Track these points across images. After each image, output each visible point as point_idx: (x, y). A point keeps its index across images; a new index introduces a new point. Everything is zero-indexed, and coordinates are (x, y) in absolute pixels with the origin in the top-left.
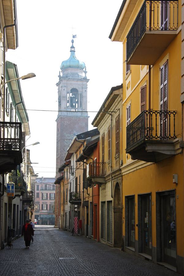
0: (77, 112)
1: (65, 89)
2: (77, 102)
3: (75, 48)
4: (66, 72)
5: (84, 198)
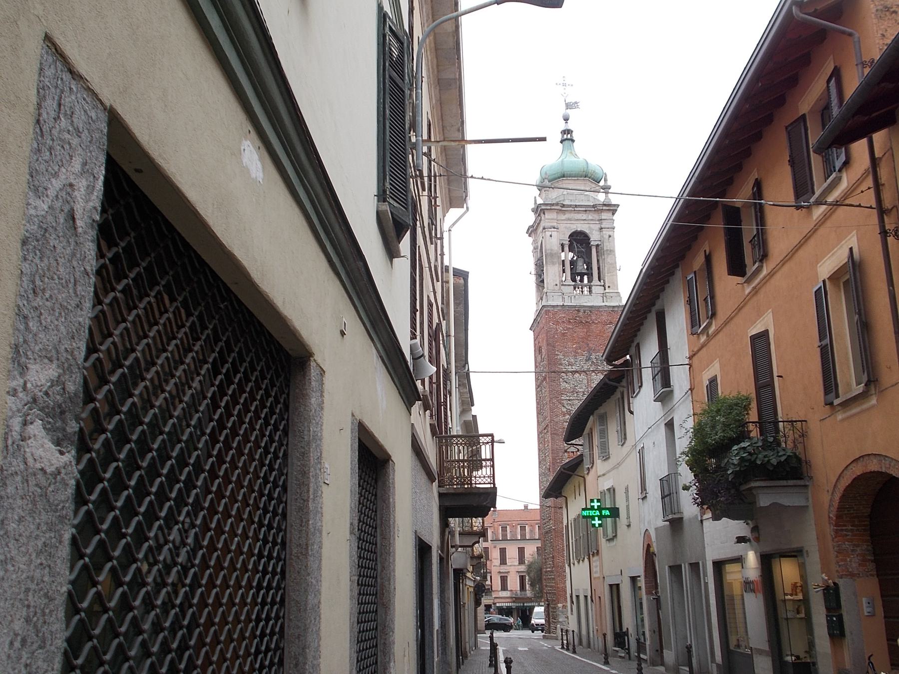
3: (572, 131)
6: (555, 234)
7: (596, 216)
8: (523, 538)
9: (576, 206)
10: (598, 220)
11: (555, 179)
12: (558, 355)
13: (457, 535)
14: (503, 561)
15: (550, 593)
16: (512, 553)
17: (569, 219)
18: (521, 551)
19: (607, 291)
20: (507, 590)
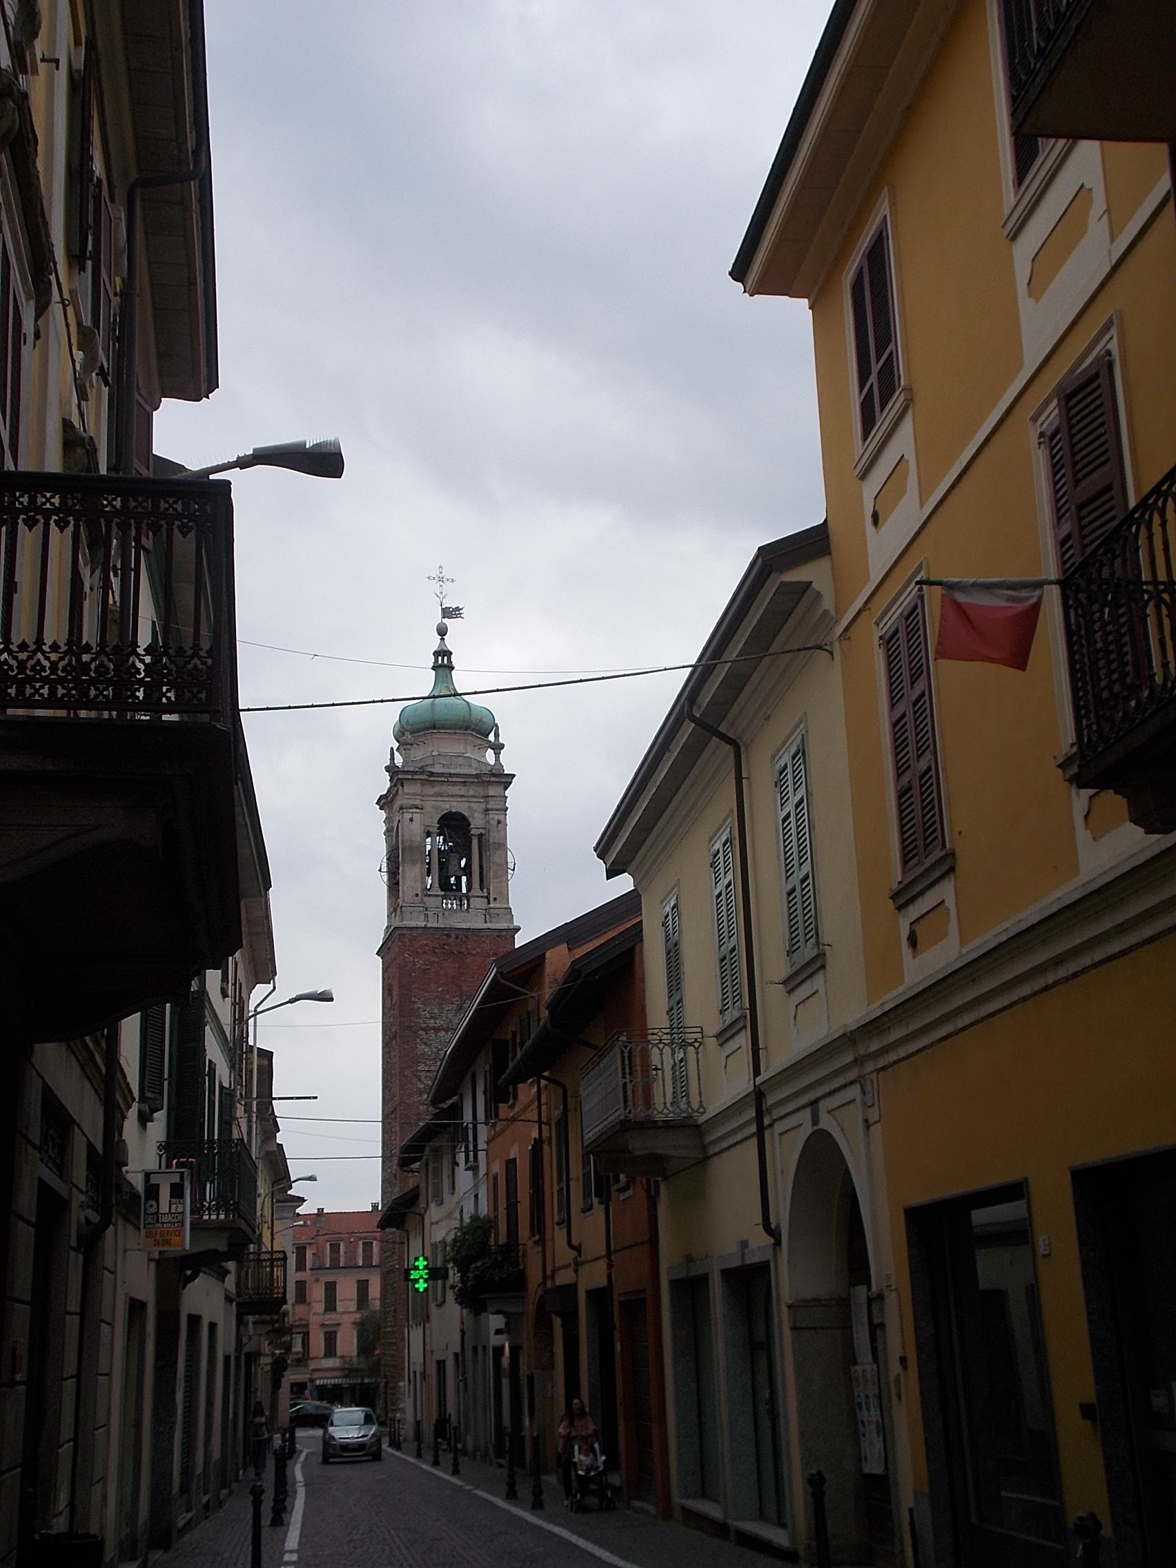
0: (343, 1268)
1: (417, 817)
2: (467, 870)
3: (451, 653)
4: (418, 754)
5: (549, 1273)
6: (417, 817)
7: (480, 791)
8: (368, 1265)
9: (450, 775)
10: (483, 797)
11: (423, 730)
12: (415, 1002)
13: (251, 1325)
14: (331, 1305)
15: (389, 1366)
16: (347, 1291)
17: (439, 795)
18: (363, 1287)
19: (492, 905)
20: (335, 1356)
